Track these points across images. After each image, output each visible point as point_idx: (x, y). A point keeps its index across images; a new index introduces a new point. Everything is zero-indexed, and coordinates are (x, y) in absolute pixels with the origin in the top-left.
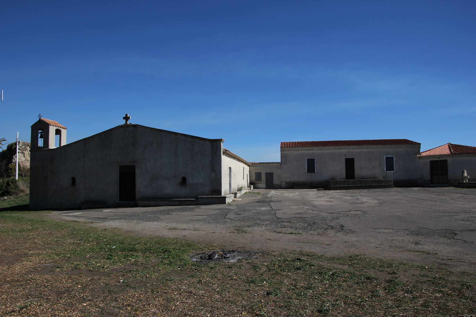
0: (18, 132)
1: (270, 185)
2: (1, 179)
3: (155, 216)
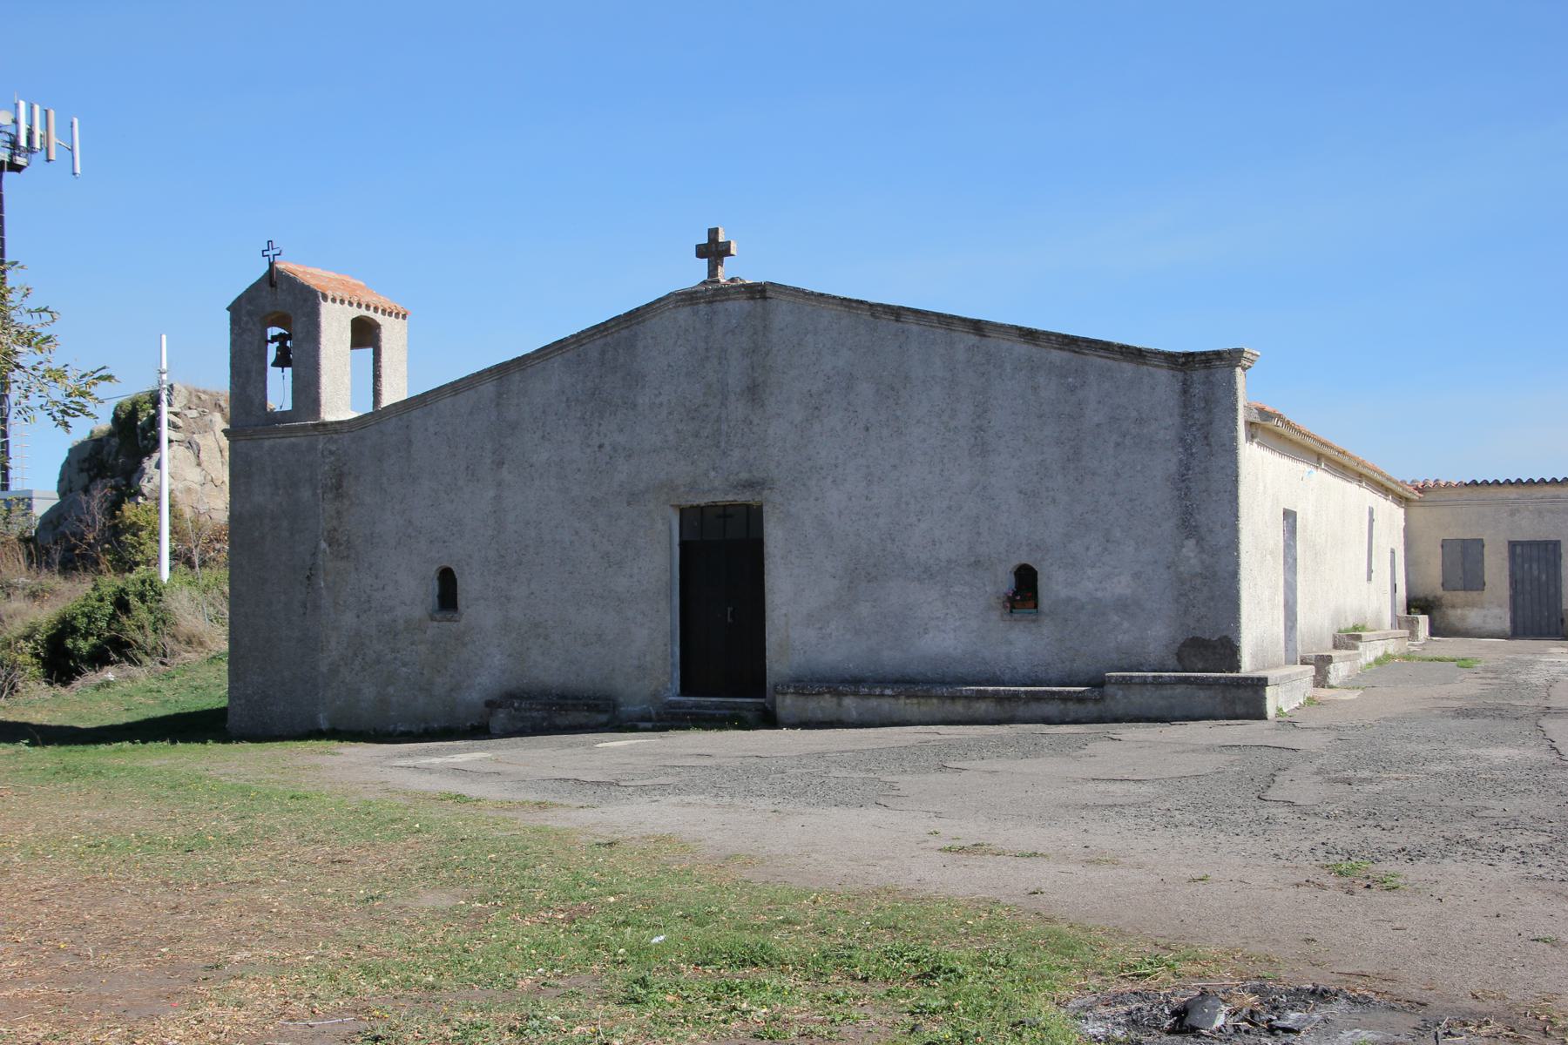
0: (164, 337)
2: (89, 579)
3: (872, 775)
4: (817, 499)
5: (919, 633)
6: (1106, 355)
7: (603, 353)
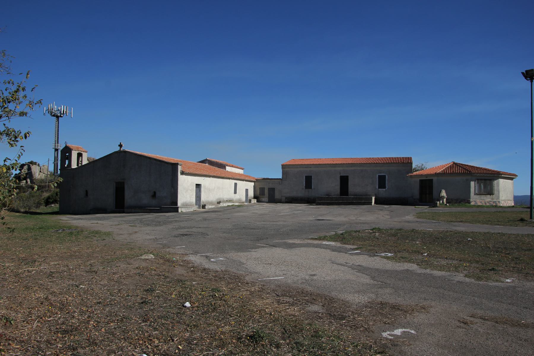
1: (272, 200)
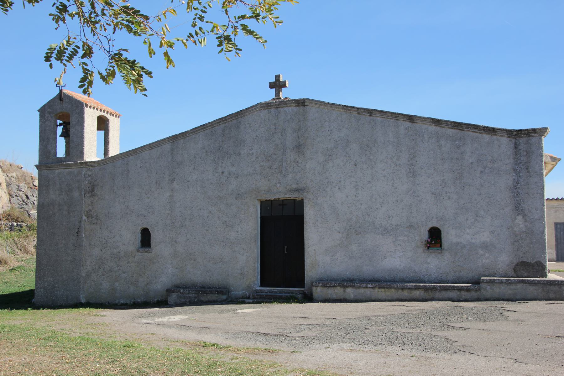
4: (331, 197)
5: (381, 258)
6: (476, 131)
7: (224, 130)
